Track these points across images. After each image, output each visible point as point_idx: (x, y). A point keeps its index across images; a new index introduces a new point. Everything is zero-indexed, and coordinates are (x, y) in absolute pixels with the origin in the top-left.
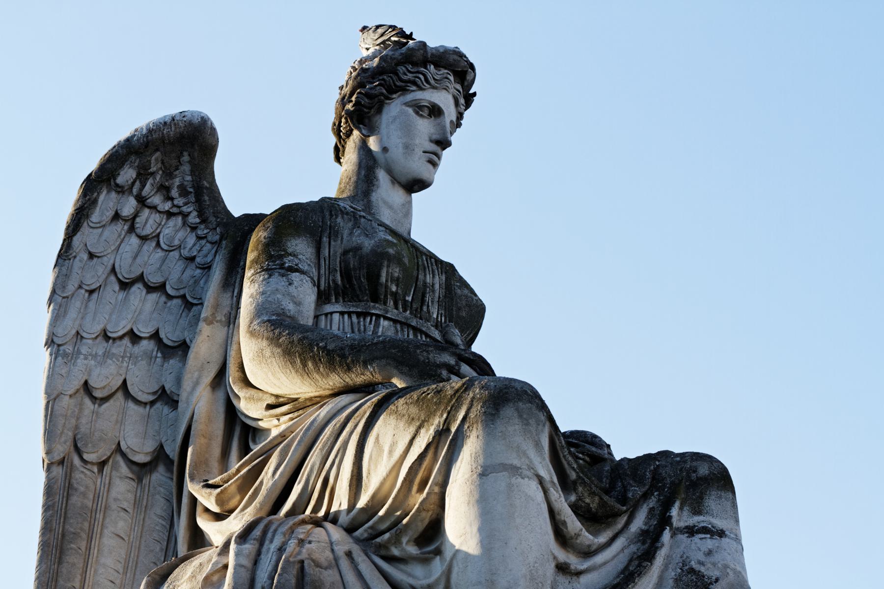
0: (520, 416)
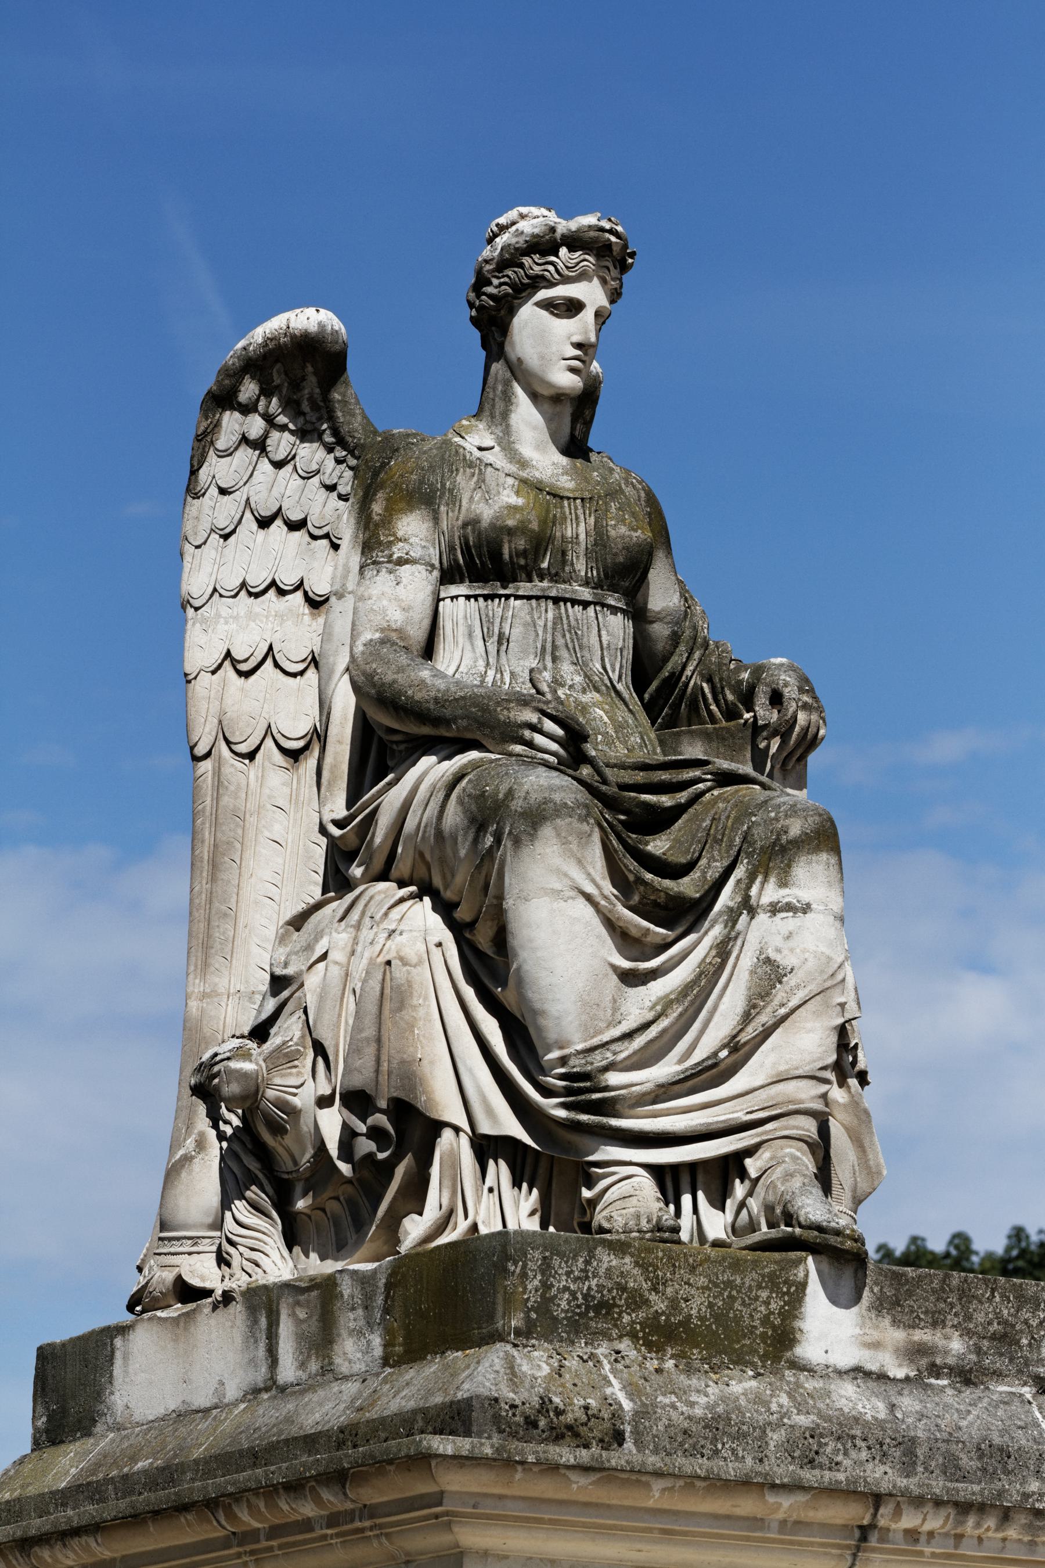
0: (558, 835)
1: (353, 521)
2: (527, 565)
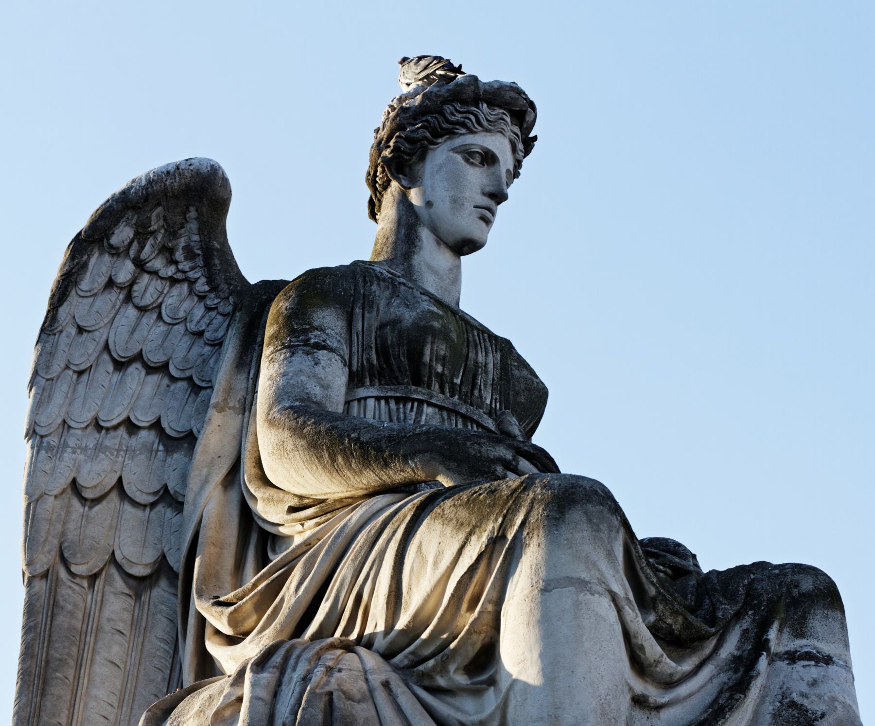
0: (590, 521)
2: (442, 374)
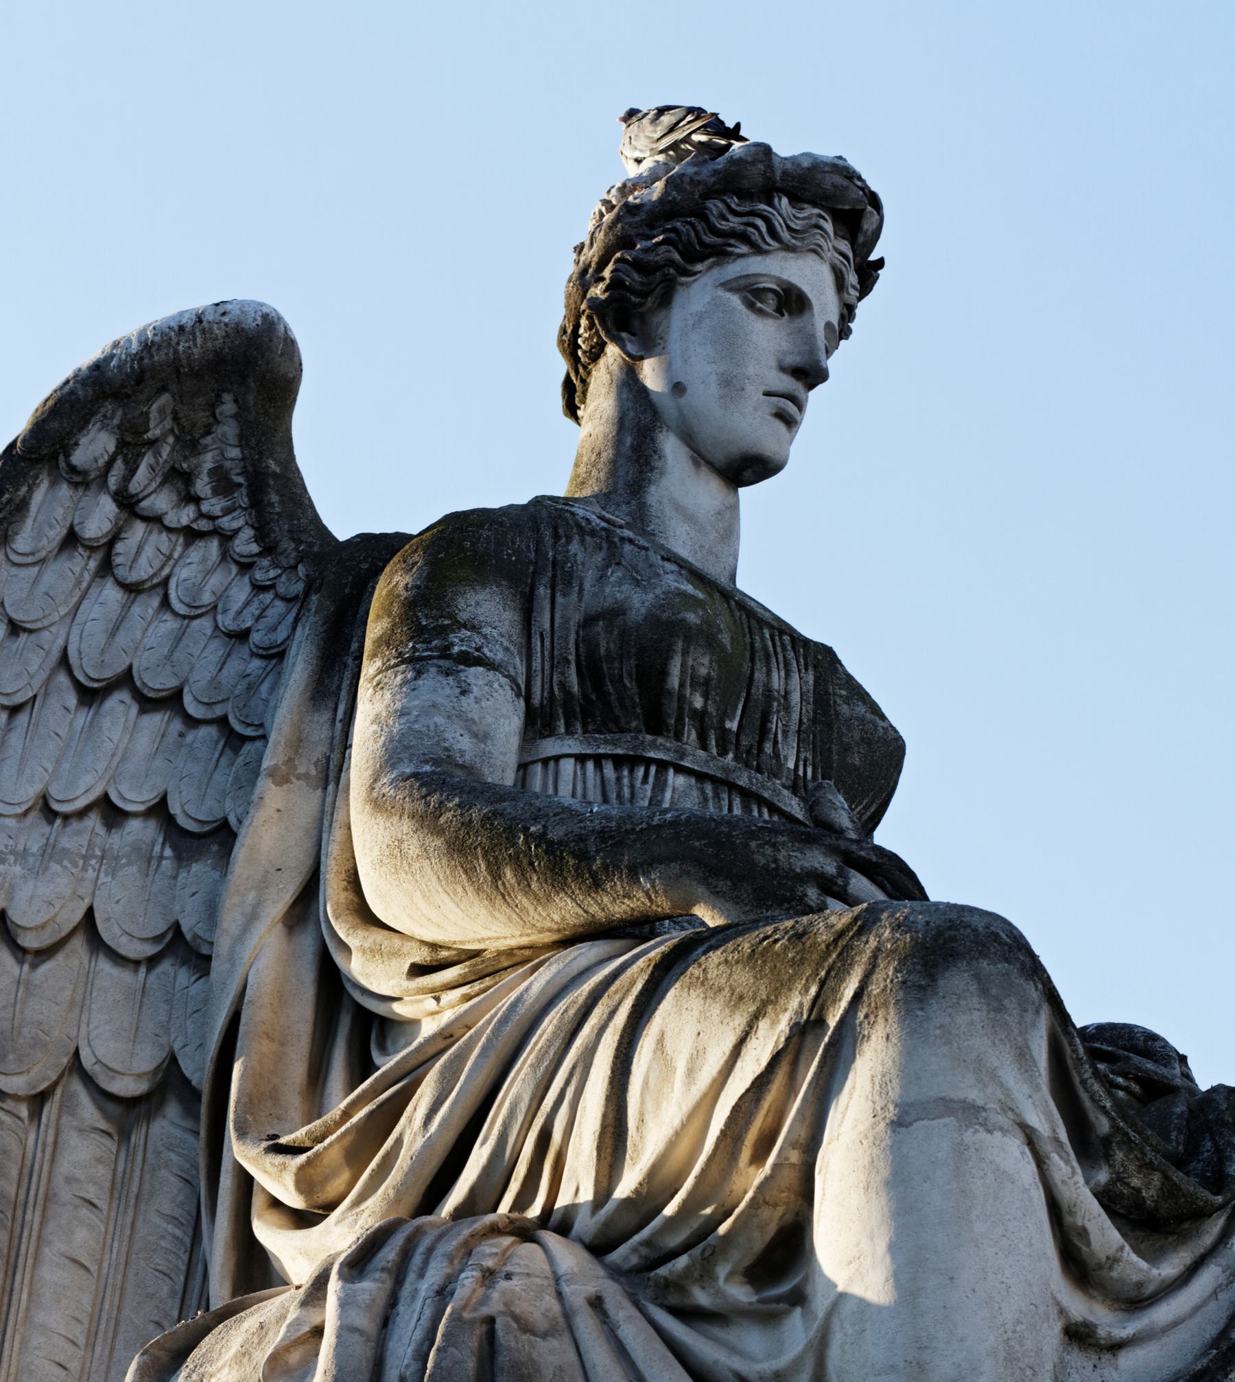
0: (984, 992)
1: (85, 947)
2: (704, 712)
